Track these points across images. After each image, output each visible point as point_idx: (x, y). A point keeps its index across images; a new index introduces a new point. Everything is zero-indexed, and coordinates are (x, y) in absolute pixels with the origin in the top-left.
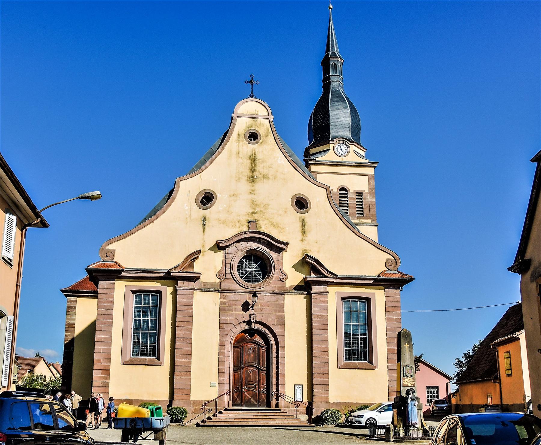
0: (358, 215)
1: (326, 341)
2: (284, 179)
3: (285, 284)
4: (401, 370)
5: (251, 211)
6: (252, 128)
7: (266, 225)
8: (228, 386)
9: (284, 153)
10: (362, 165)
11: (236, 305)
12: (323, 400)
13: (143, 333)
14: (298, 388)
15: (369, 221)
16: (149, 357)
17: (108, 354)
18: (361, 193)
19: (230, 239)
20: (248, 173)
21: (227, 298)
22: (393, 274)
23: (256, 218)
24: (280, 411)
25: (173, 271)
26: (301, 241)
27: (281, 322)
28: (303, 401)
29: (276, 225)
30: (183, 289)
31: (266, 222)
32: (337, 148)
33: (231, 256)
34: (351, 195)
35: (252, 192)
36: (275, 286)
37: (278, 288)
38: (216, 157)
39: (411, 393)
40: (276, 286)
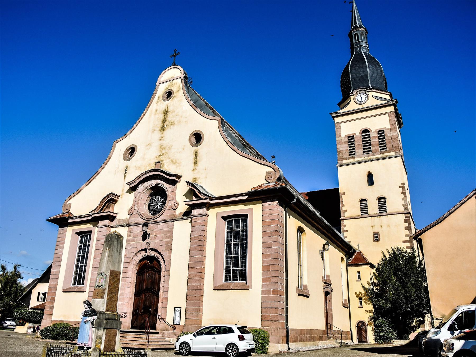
0: (381, 151)
1: (203, 263)
2: (186, 121)
3: (175, 212)
5: (159, 154)
7: (168, 164)
9: (188, 100)
12: (193, 323)
13: (230, 267)
14: (178, 311)
15: (393, 154)
17: (56, 284)
18: (383, 130)
19: (135, 180)
20: (160, 124)
21: (132, 231)
23: (162, 159)
24: (158, 333)
26: (193, 171)
28: (181, 324)
29: (175, 162)
30: (100, 227)
31: (168, 160)
32: (358, 98)
34: (373, 134)
36: (168, 215)
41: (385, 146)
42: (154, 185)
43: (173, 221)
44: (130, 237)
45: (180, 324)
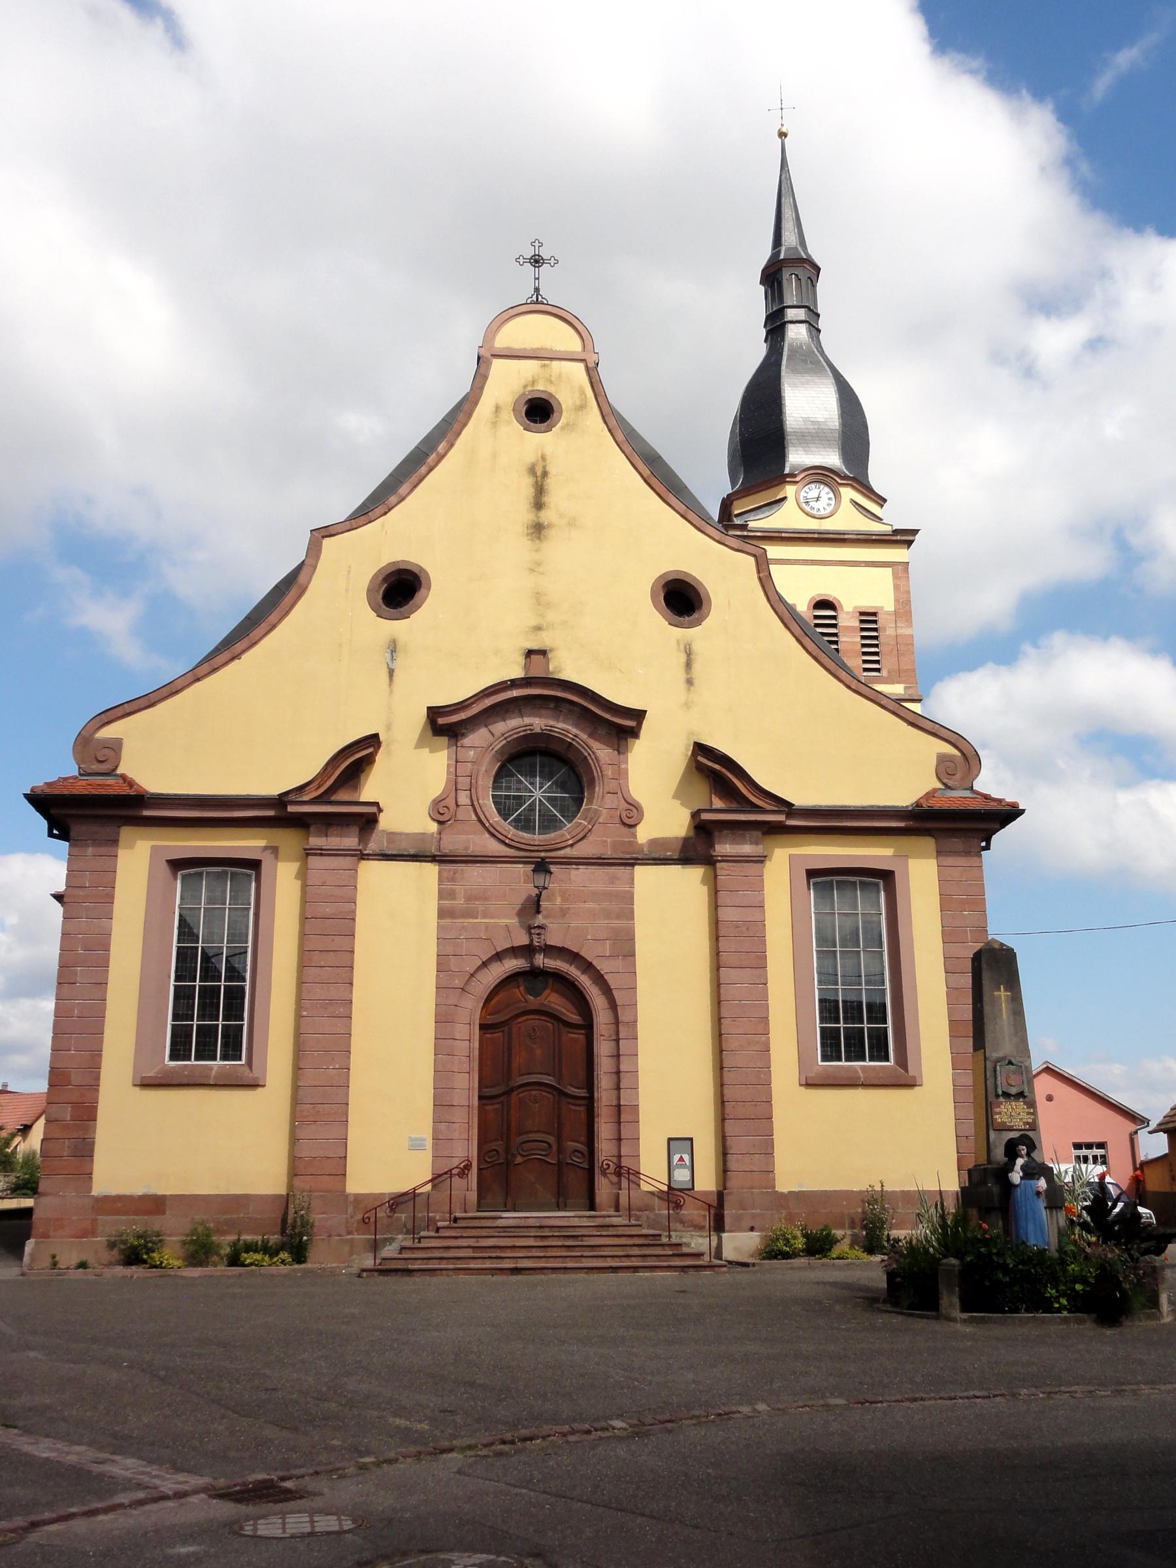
4: (988, 1074)
5: (533, 622)
6: (535, 388)
8: (465, 1148)
10: (874, 537)
11: (486, 899)
16: (222, 1063)
18: (874, 614)
20: (525, 515)
22: (957, 798)
25: (292, 797)
27: (625, 948)
33: (472, 753)
34: (847, 620)
35: (535, 568)
36: (606, 842)
37: (615, 845)
38: (431, 470)
39: (1024, 1152)
40: (609, 840)
41: (877, 662)
42: (538, 730)
43: (633, 865)
44: (454, 899)
45: (693, 1188)
